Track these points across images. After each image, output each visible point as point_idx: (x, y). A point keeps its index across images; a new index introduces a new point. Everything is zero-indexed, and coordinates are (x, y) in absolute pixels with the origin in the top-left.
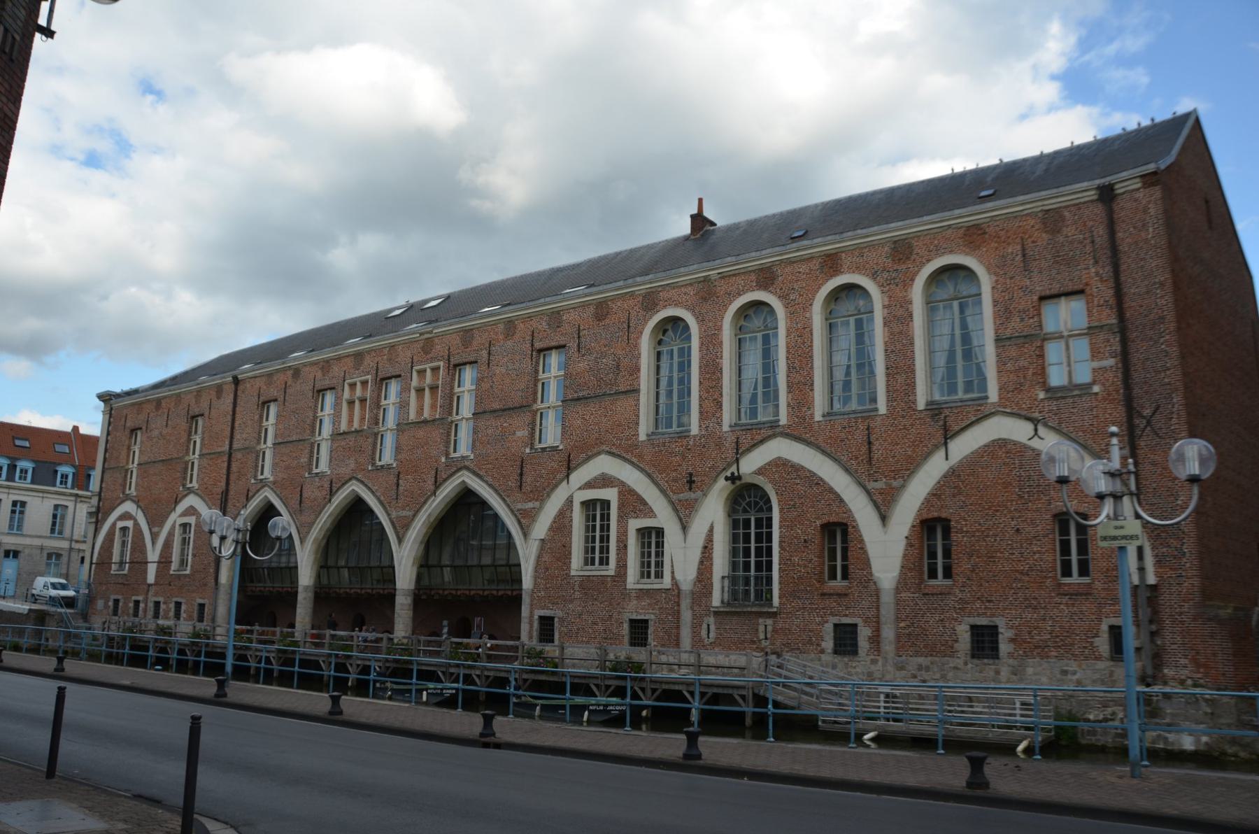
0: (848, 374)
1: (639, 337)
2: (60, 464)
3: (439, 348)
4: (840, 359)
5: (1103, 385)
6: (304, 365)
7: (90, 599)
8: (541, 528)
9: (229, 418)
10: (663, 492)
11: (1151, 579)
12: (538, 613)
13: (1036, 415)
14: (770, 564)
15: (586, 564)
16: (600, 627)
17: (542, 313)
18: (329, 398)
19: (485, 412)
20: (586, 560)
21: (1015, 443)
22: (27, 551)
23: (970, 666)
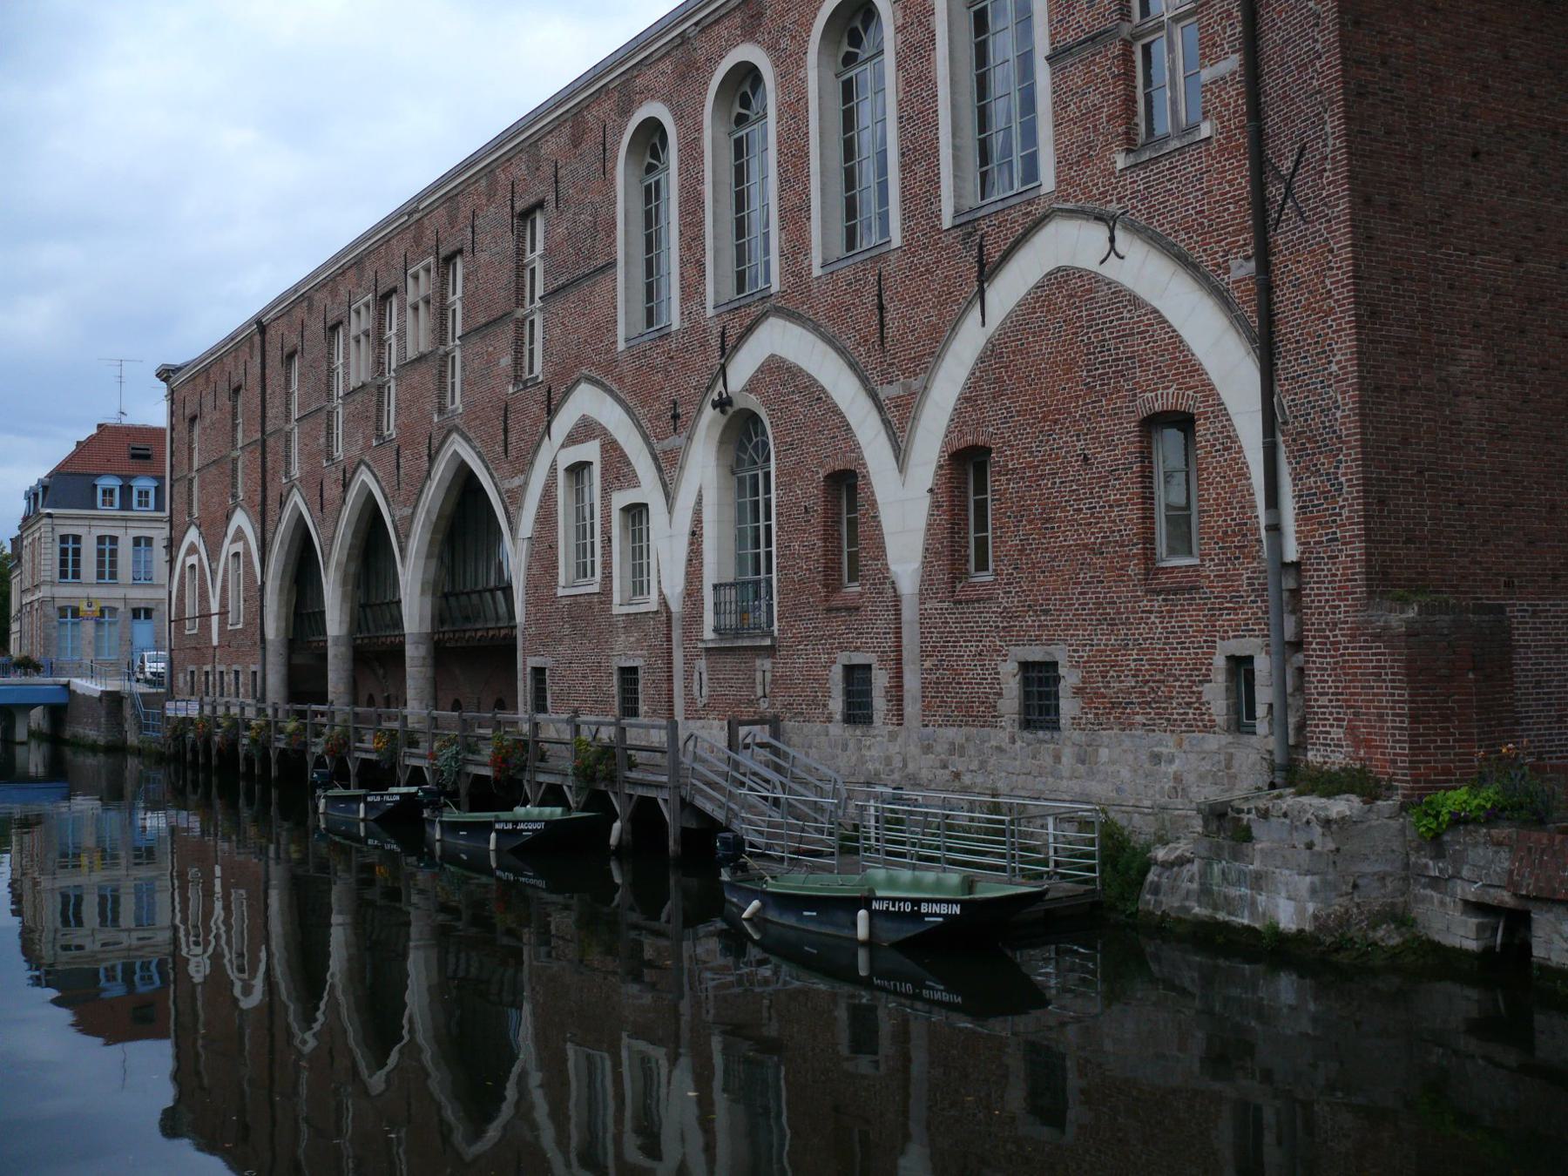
1: (614, 167)
5: (1220, 117)
10: (646, 438)
11: (1292, 553)
13: (1114, 207)
16: (590, 682)
23: (1019, 743)
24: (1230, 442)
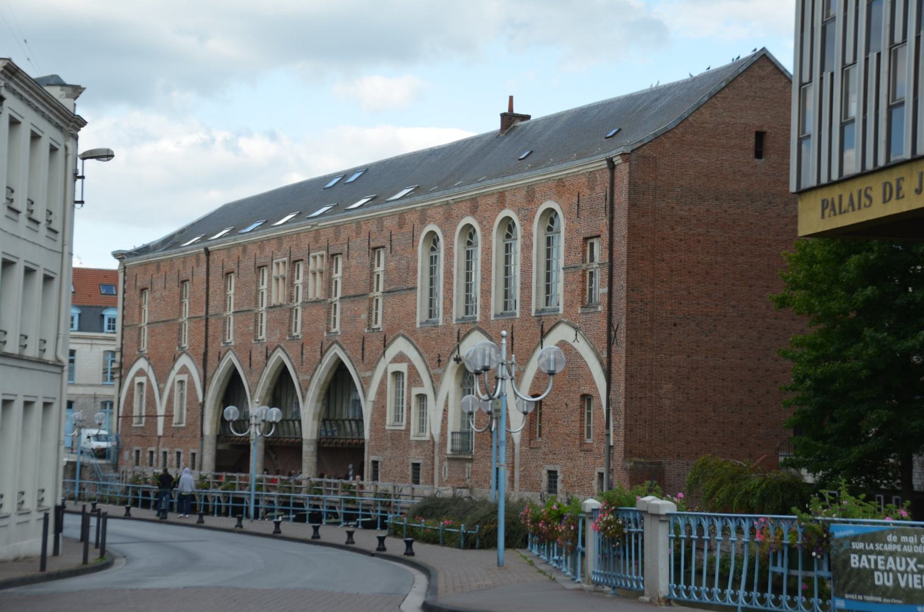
2: (106, 308)
7: (119, 450)
9: (205, 286)
16: (399, 469)
17: (372, 218)
22: (80, 401)
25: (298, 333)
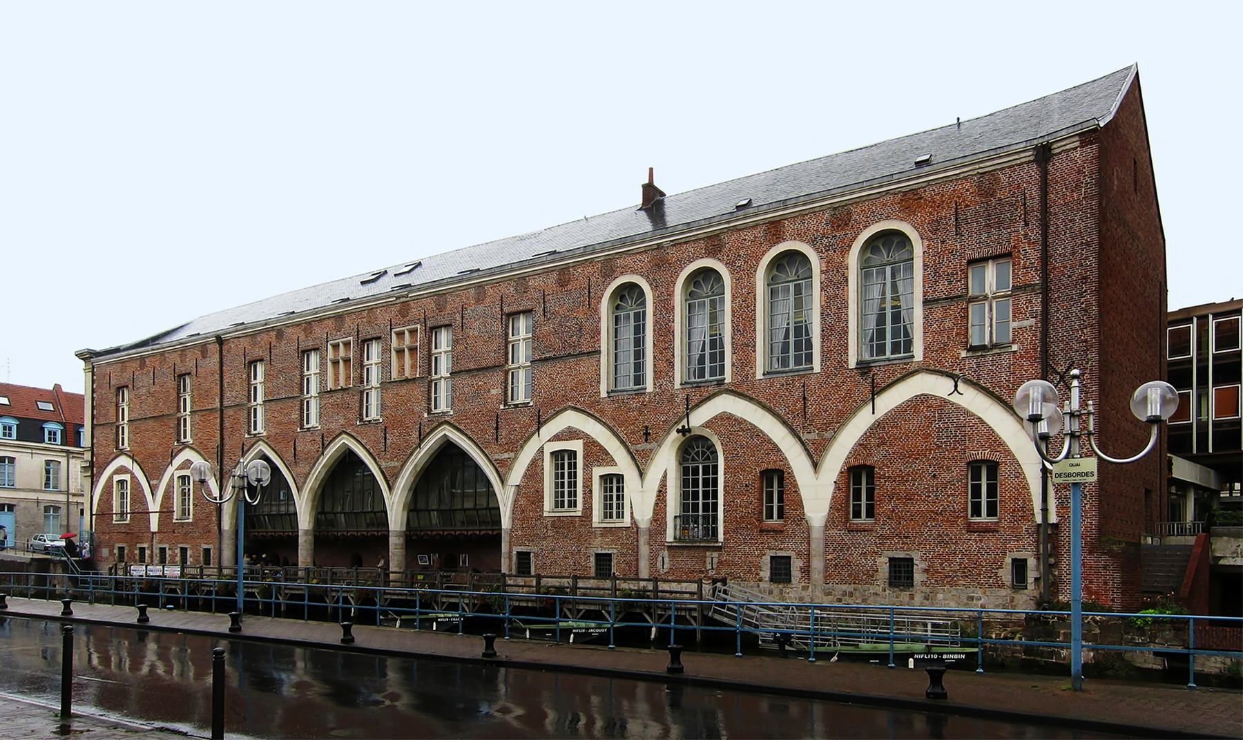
0: (787, 336)
3: (415, 312)
4: (780, 323)
5: (1022, 343)
6: (287, 326)
8: (517, 475)
9: (218, 377)
10: (623, 443)
11: (1053, 519)
12: (516, 549)
13: (957, 372)
14: (715, 506)
15: (557, 506)
18: (314, 359)
19: (460, 372)
20: (557, 502)
21: (936, 398)
22: (22, 505)
24: (1019, 474)
25: (374, 414)
